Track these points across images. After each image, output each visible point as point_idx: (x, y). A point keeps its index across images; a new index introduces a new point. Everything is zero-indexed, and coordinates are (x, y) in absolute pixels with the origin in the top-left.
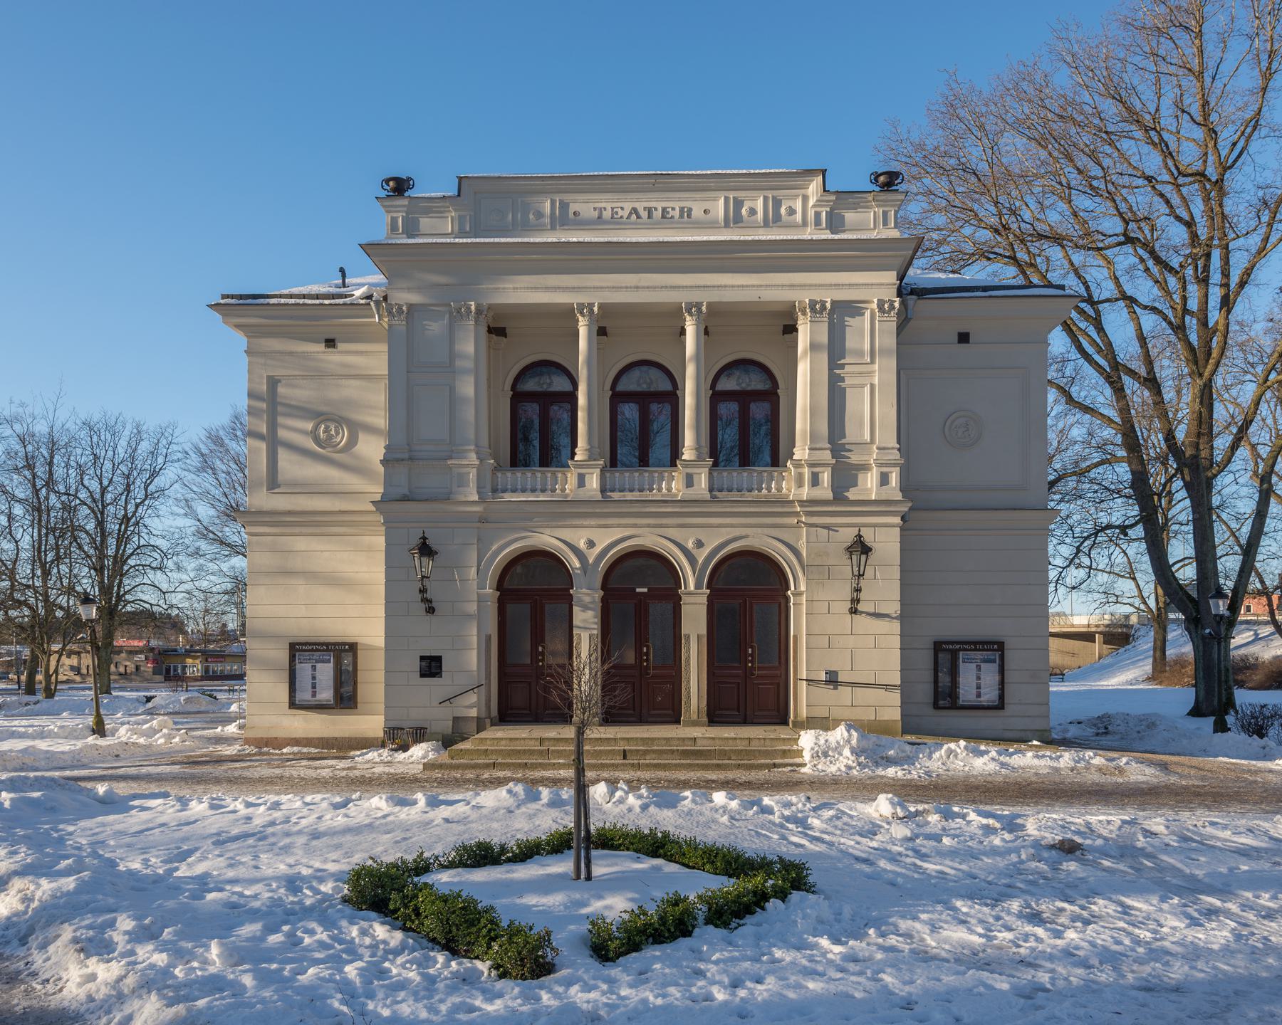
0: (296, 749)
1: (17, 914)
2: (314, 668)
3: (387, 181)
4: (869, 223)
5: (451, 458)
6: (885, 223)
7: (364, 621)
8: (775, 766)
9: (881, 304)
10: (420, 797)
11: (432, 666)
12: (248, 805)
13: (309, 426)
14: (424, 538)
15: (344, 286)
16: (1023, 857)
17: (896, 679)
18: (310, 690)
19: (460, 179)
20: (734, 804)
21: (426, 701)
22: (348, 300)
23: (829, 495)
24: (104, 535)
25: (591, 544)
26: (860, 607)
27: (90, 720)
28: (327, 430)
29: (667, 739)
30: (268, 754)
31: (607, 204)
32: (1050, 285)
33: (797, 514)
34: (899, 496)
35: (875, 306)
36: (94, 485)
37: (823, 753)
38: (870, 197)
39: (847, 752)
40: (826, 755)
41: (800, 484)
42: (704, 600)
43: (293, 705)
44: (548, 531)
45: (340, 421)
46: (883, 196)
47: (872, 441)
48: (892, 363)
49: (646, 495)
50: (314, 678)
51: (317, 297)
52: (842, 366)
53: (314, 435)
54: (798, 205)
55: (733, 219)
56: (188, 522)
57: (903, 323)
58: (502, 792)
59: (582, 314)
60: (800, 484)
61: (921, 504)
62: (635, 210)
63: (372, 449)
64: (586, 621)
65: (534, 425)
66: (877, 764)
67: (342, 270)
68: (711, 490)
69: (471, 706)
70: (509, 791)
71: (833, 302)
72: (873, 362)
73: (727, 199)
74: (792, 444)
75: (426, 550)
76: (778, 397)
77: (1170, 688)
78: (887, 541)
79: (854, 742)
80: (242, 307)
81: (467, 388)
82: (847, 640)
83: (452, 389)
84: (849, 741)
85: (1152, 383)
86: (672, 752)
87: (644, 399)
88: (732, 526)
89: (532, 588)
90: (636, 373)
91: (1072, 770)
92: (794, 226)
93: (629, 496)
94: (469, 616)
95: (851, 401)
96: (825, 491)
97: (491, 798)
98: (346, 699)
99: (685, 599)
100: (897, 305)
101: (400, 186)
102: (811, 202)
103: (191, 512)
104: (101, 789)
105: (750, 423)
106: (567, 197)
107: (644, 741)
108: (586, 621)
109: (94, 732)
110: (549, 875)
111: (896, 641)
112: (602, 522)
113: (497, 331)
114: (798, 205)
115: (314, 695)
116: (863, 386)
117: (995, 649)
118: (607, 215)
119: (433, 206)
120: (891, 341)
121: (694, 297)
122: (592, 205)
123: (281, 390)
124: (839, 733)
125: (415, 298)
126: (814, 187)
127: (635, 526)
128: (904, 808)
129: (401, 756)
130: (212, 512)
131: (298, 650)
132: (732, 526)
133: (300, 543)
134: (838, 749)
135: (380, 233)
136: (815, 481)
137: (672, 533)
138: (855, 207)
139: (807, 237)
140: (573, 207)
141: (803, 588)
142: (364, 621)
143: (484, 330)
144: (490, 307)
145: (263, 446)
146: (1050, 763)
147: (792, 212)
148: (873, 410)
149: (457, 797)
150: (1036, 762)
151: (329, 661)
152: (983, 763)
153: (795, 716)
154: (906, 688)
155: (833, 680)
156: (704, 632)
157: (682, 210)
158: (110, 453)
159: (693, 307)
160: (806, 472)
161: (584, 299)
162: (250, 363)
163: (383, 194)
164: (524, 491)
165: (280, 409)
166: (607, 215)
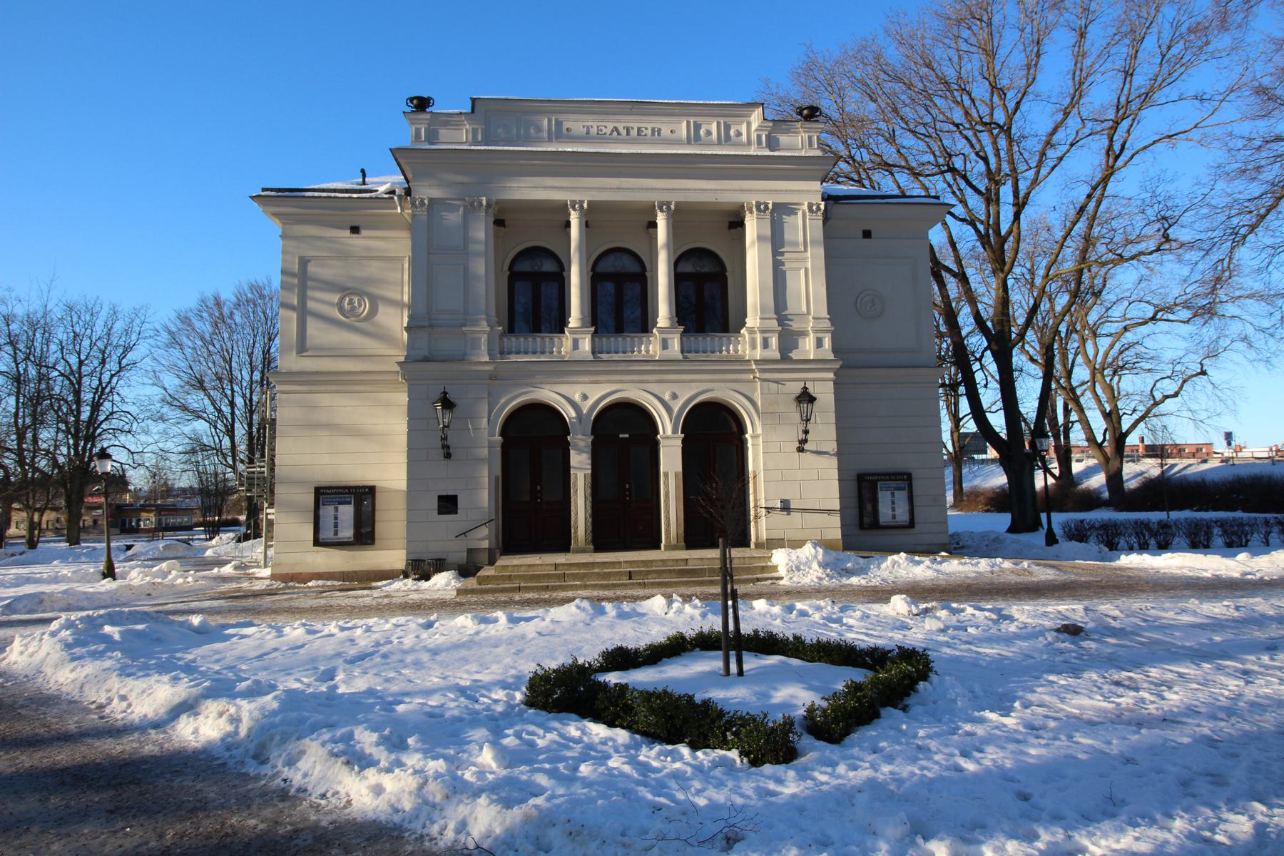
0: (320, 582)
1: (229, 735)
2: (336, 510)
3: (412, 100)
4: (800, 142)
5: (465, 325)
6: (810, 144)
7: (388, 470)
8: (758, 580)
9: (810, 206)
10: (500, 614)
11: (448, 504)
12: (343, 629)
13: (335, 298)
14: (445, 393)
15: (364, 183)
16: (1050, 639)
17: (836, 505)
18: (890, 506)
19: (474, 100)
20: (776, 609)
21: (444, 535)
22: (373, 195)
23: (777, 355)
24: (78, 402)
25: (585, 397)
26: (806, 447)
27: (102, 566)
28: (351, 302)
29: (664, 561)
30: (294, 588)
31: (594, 123)
32: (929, 196)
33: (752, 371)
34: (832, 357)
35: (805, 207)
36: (73, 360)
37: (796, 568)
38: (799, 125)
39: (815, 566)
40: (798, 569)
41: (753, 347)
42: (679, 443)
43: (317, 542)
44: (548, 386)
45: (361, 294)
46: (808, 125)
47: (808, 313)
48: (821, 251)
49: (629, 356)
50: (336, 518)
51: (346, 191)
52: (782, 254)
53: (340, 306)
54: (744, 129)
55: (694, 138)
56: (157, 390)
57: (826, 218)
58: (571, 608)
59: (574, 209)
60: (753, 347)
61: (850, 362)
62: (616, 129)
63: (396, 321)
64: (580, 463)
65: (531, 299)
66: (841, 576)
67: (363, 171)
68: (682, 352)
69: (483, 539)
70: (578, 607)
71: (774, 204)
72: (806, 250)
73: (688, 123)
74: (744, 315)
75: (447, 404)
76: (726, 278)
77: (970, 514)
78: (824, 391)
79: (820, 557)
80: (283, 200)
81: (480, 267)
82: (791, 474)
83: (466, 269)
84: (816, 557)
85: (962, 278)
86: (670, 571)
87: (619, 278)
88: (701, 381)
89: (534, 434)
90: (611, 258)
91: (992, 572)
92: (740, 145)
93: (616, 357)
94: (481, 460)
95: (786, 278)
96: (774, 352)
97: (565, 614)
98: (365, 536)
99: (662, 443)
100: (822, 207)
101: (422, 104)
102: (754, 127)
103: (157, 383)
104: (196, 620)
105: (708, 301)
106: (562, 117)
107: (644, 563)
108: (580, 463)
109: (105, 576)
110: (765, 667)
111: (835, 474)
112: (593, 378)
113: (499, 223)
114: (744, 129)
115: (336, 533)
116: (799, 269)
117: (904, 479)
118: (594, 131)
119: (449, 120)
120: (819, 234)
121: (665, 197)
122: (581, 124)
123: (312, 269)
124: (808, 550)
125: (436, 193)
126: (756, 117)
127: (621, 382)
128: (917, 607)
129: (424, 585)
130: (177, 381)
131: (325, 494)
132: (701, 381)
133: (325, 399)
134: (808, 564)
135: (406, 141)
136: (766, 344)
137: (653, 387)
138: (787, 132)
139: (752, 153)
140: (566, 125)
141: (759, 431)
142: (388, 470)
143: (491, 220)
144: (498, 202)
145: (294, 315)
146: (972, 568)
147: (739, 134)
148: (809, 289)
149: (530, 614)
150: (961, 568)
151: (349, 503)
152: (922, 570)
153: (757, 538)
154: (842, 511)
155: (786, 507)
156: (679, 468)
157: (653, 130)
158: (89, 331)
159: (665, 206)
160: (759, 337)
161: (577, 197)
162: (284, 246)
163: (409, 109)
164: (526, 353)
165: (309, 283)
166: (594, 131)
